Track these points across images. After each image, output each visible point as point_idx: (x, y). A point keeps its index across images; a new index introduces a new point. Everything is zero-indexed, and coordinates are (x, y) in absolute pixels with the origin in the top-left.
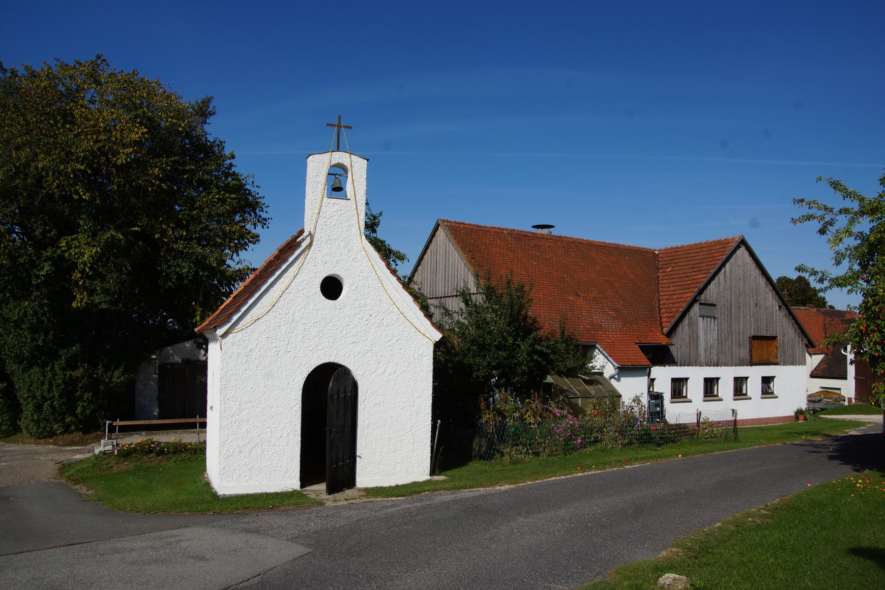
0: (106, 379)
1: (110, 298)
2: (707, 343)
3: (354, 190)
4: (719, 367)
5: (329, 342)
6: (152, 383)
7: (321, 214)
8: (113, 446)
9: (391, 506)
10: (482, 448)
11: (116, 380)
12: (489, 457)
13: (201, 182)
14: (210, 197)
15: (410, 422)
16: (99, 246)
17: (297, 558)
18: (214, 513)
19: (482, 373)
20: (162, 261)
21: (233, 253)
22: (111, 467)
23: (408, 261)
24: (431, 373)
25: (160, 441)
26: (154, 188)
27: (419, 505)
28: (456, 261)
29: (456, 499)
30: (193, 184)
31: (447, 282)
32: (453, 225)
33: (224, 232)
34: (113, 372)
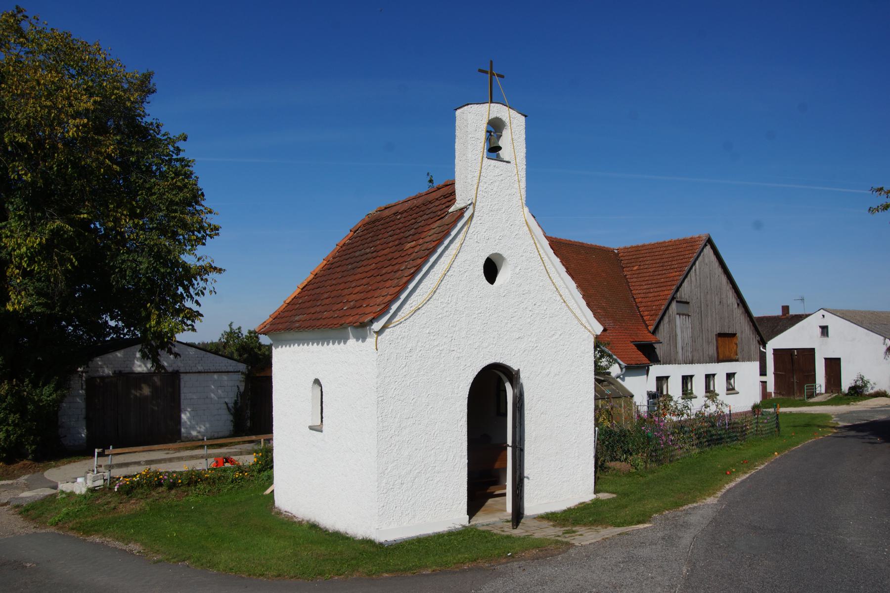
2: (683, 341)
4: (693, 364)
5: (494, 338)
7: (482, 178)
11: (46, 398)
15: (575, 432)
22: (114, 508)
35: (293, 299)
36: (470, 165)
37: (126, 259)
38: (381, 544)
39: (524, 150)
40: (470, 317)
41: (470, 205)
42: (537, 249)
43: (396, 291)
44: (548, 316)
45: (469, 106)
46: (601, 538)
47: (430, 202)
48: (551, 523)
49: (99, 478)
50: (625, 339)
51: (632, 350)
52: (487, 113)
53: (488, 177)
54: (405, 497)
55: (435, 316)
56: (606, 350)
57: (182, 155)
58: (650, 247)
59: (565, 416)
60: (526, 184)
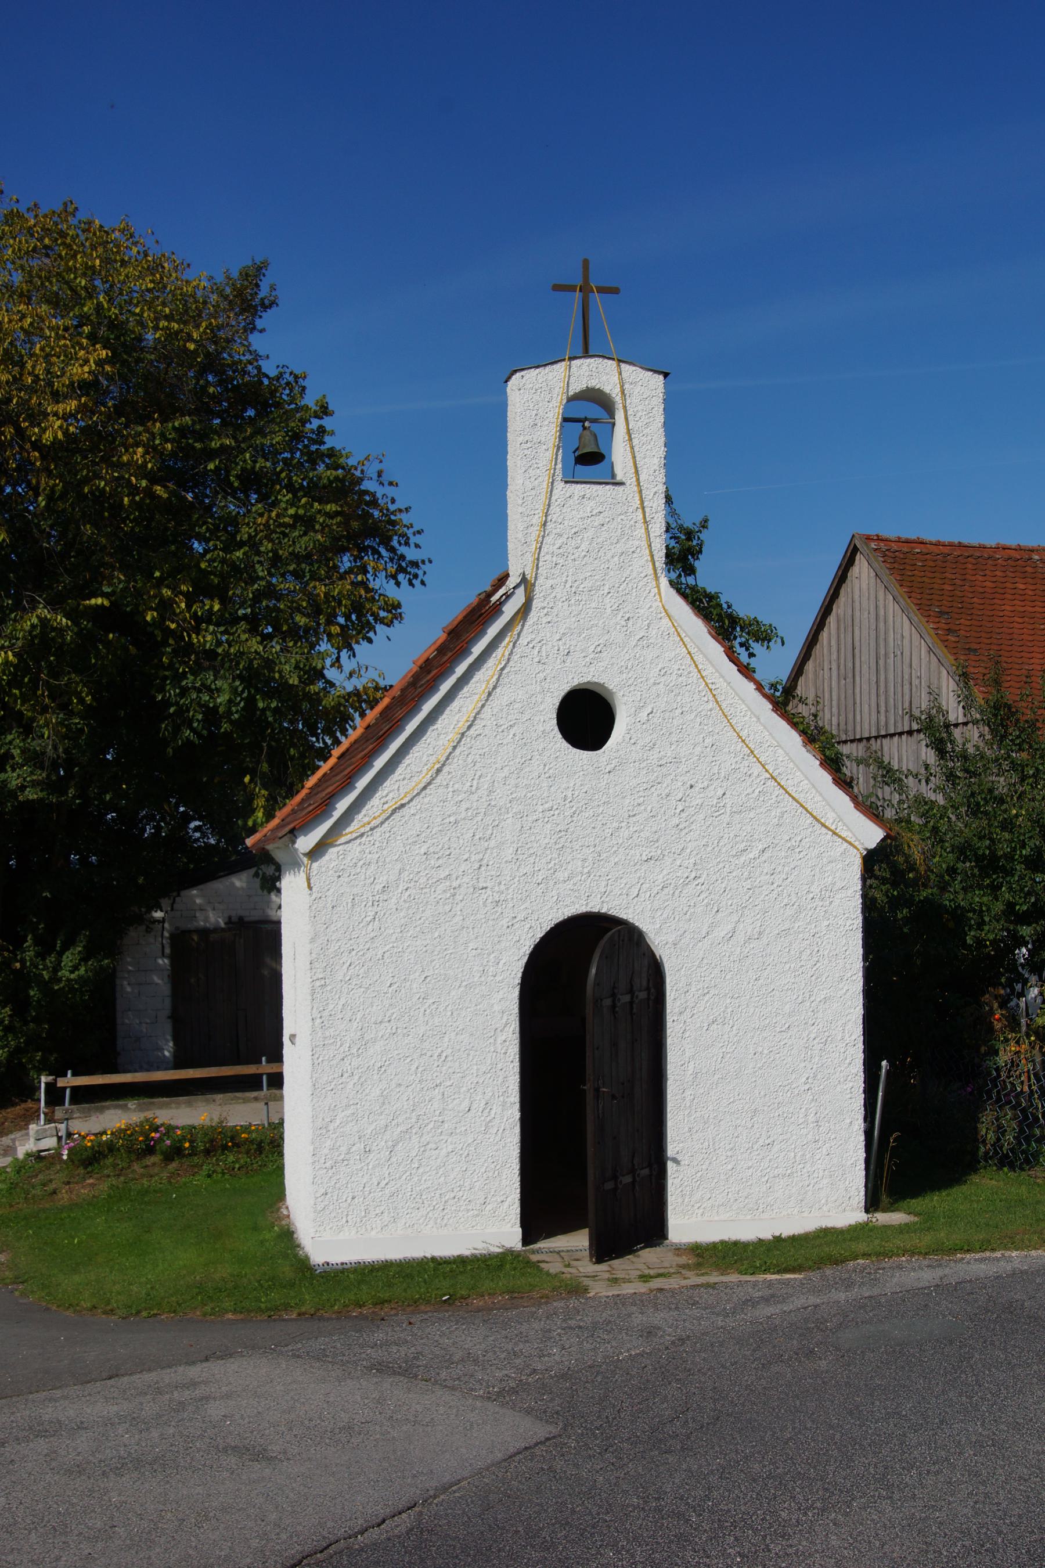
0: (44, 973)
1: (44, 775)
3: (634, 457)
5: (584, 860)
6: (156, 979)
8: (60, 1138)
9: (766, 1300)
10: (1003, 1135)
11: (67, 974)
12: (1027, 1161)
13: (252, 481)
14: (274, 514)
16: (11, 647)
17: (515, 1455)
18: (299, 1315)
19: (993, 931)
20: (166, 678)
21: (339, 650)
22: (54, 1192)
23: (783, 644)
24: (859, 935)
25: (173, 1123)
26: (137, 498)
27: (842, 1296)
28: (906, 642)
29: (946, 1281)
30: (231, 485)
31: (882, 698)
32: (894, 546)
33: (312, 598)
34: (61, 954)
36: (520, 502)
37: (190, 685)
39: (661, 451)
40: (525, 818)
44: (728, 810)
49: (48, 1133)
55: (439, 819)
59: (778, 1029)
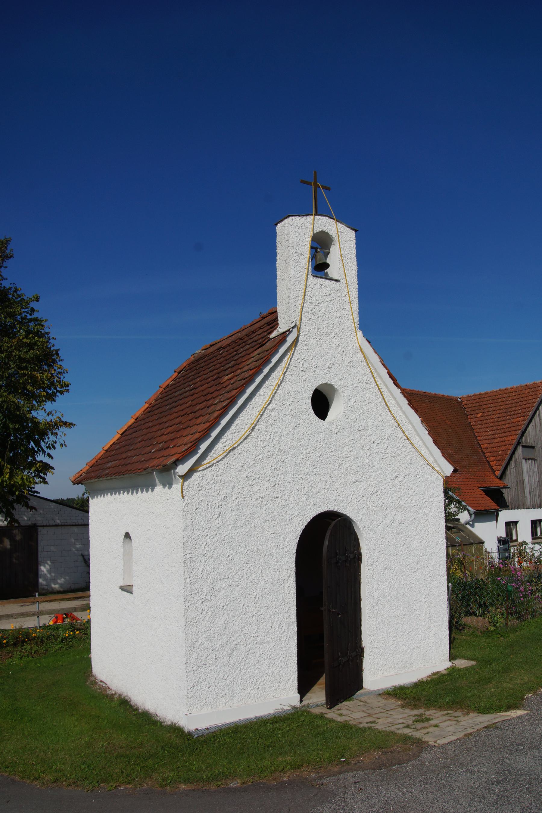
2: (530, 485)
5: (326, 482)
7: (307, 298)
35: (111, 446)
36: (292, 283)
38: (190, 734)
39: (355, 268)
40: (297, 457)
41: (293, 328)
42: (374, 379)
43: (205, 427)
45: (290, 218)
46: (463, 734)
47: (252, 332)
48: (399, 703)
50: (472, 485)
51: (480, 496)
52: (312, 226)
53: (314, 297)
54: (221, 675)
55: (254, 457)
56: (455, 496)
57: (35, 315)
58: (492, 394)
59: (413, 571)
60: (359, 306)
